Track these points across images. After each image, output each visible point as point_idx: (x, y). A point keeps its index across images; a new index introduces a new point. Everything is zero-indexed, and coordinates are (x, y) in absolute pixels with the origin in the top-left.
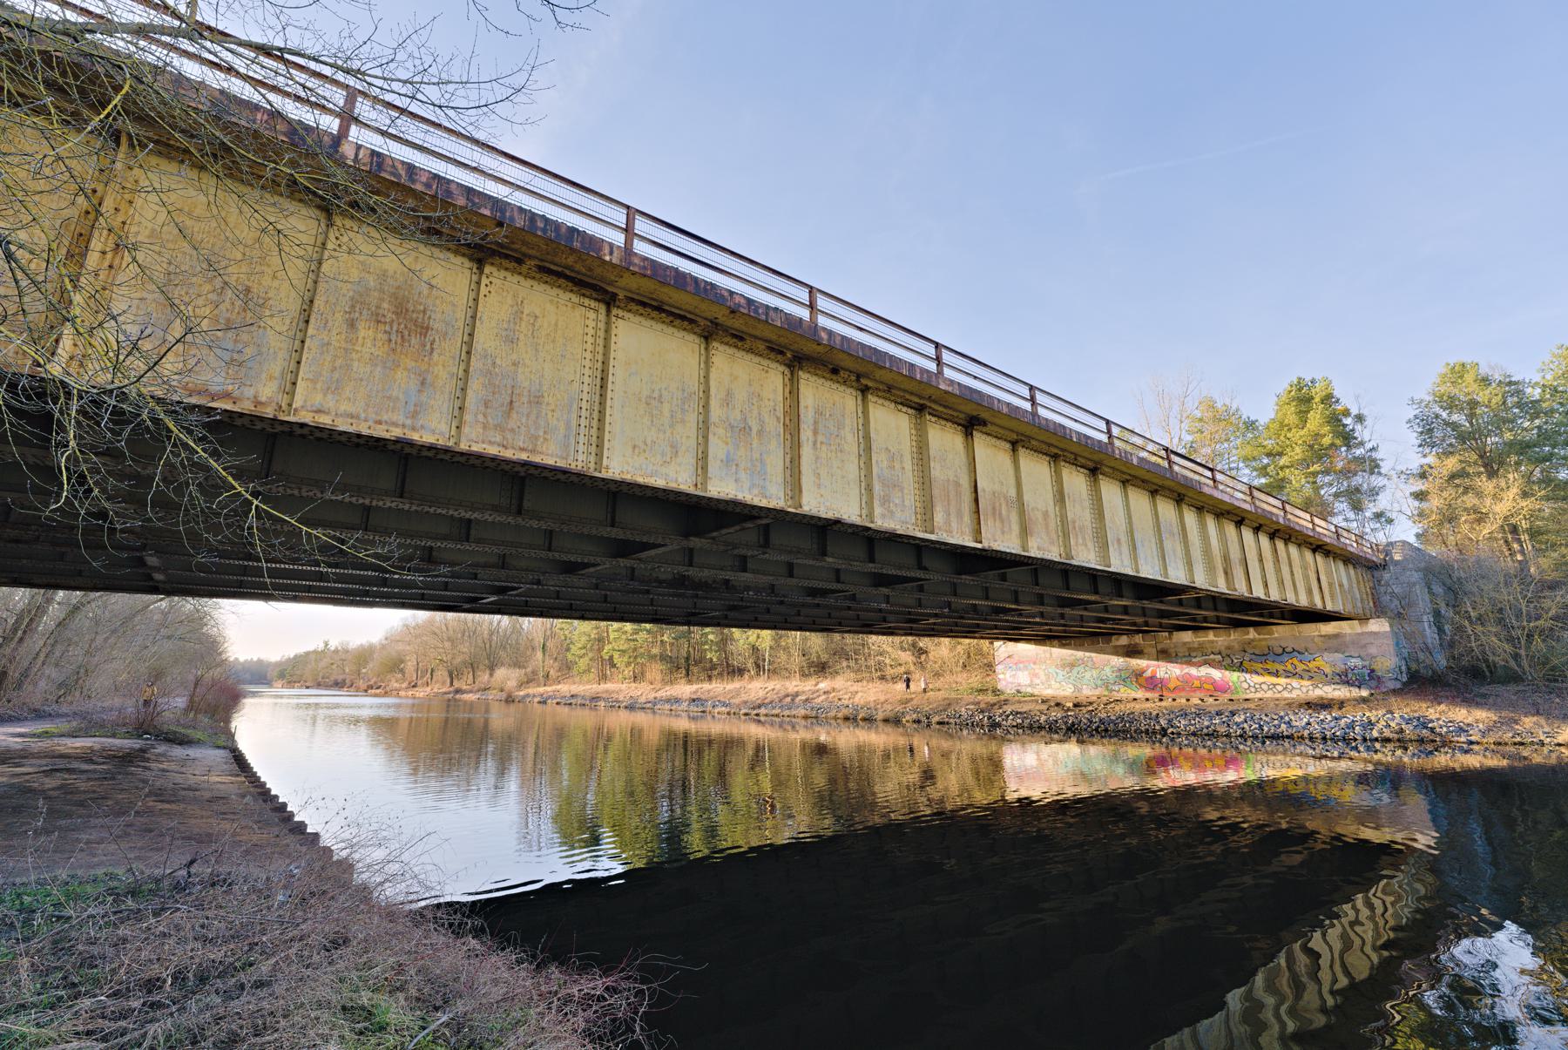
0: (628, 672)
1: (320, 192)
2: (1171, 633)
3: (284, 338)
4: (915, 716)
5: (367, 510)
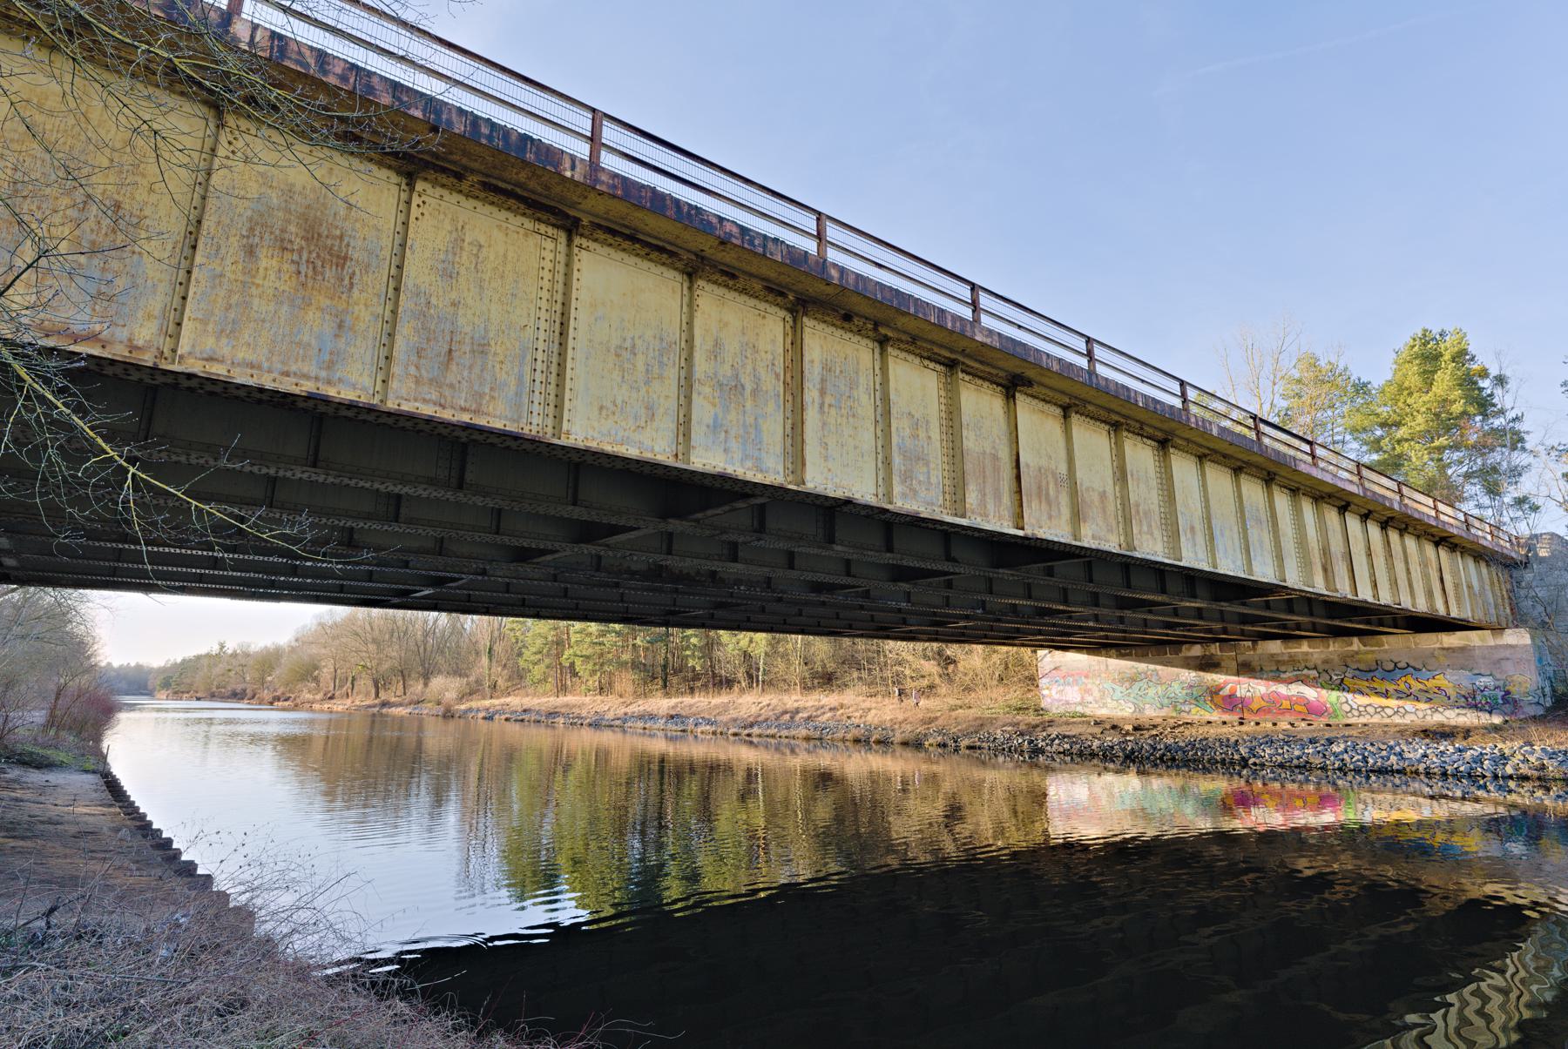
0: (593, 682)
1: (207, 83)
2: (1255, 642)
3: (165, 267)
4: (939, 739)
5: (273, 481)
